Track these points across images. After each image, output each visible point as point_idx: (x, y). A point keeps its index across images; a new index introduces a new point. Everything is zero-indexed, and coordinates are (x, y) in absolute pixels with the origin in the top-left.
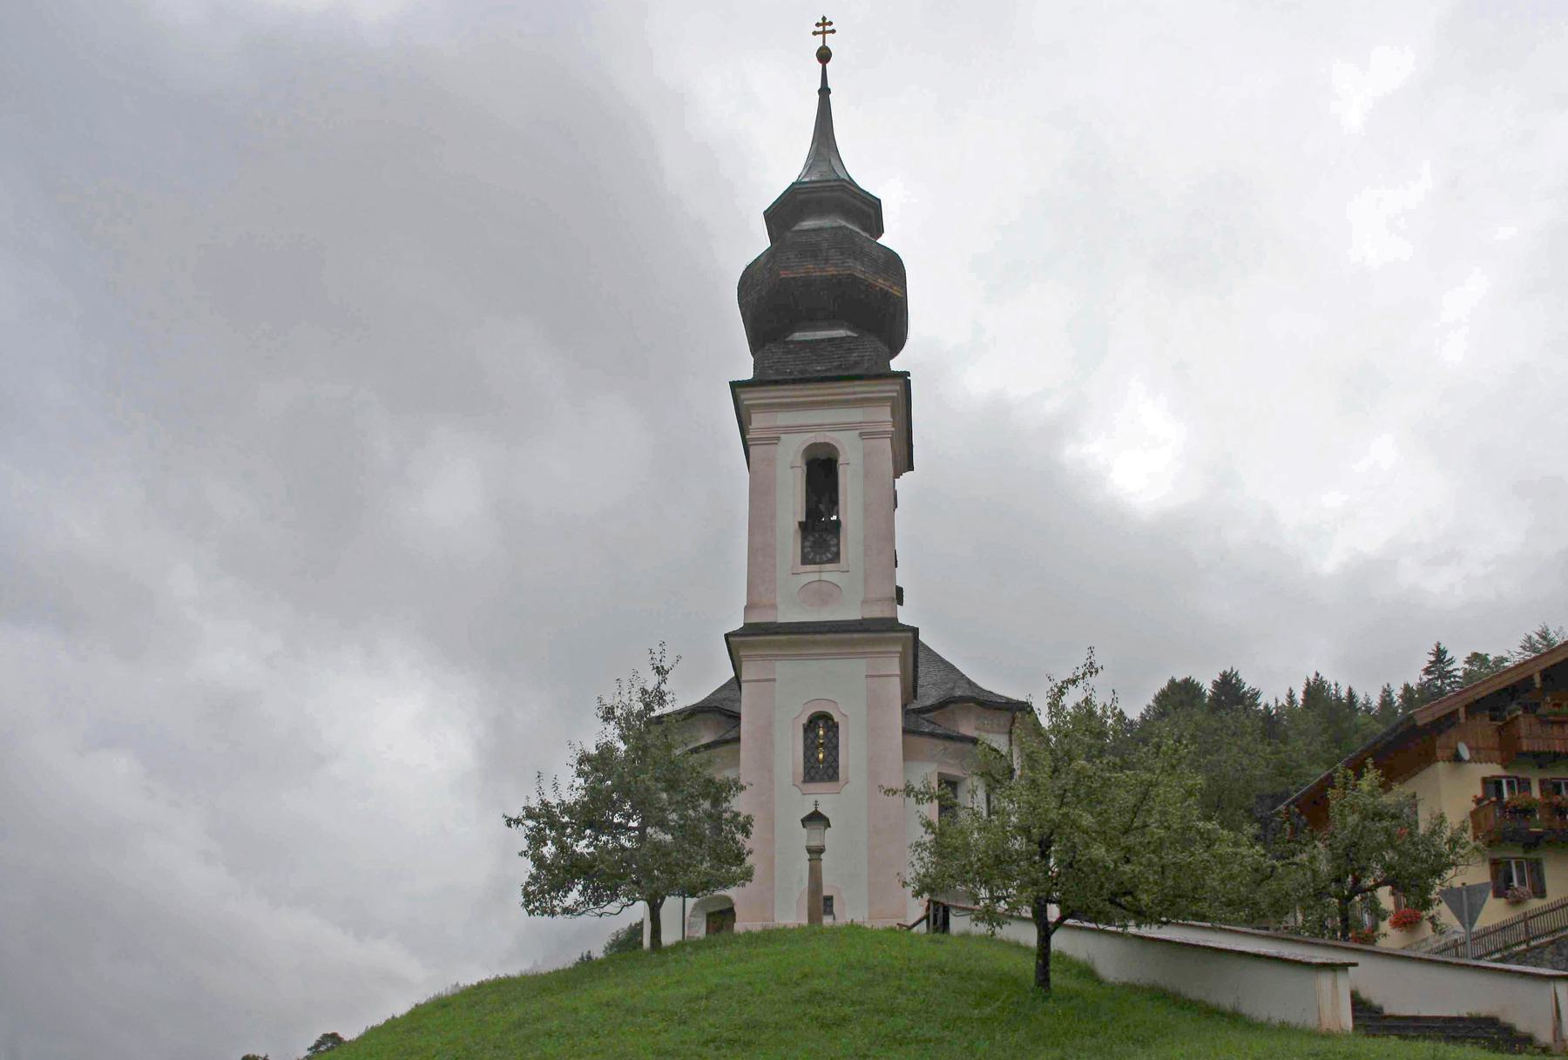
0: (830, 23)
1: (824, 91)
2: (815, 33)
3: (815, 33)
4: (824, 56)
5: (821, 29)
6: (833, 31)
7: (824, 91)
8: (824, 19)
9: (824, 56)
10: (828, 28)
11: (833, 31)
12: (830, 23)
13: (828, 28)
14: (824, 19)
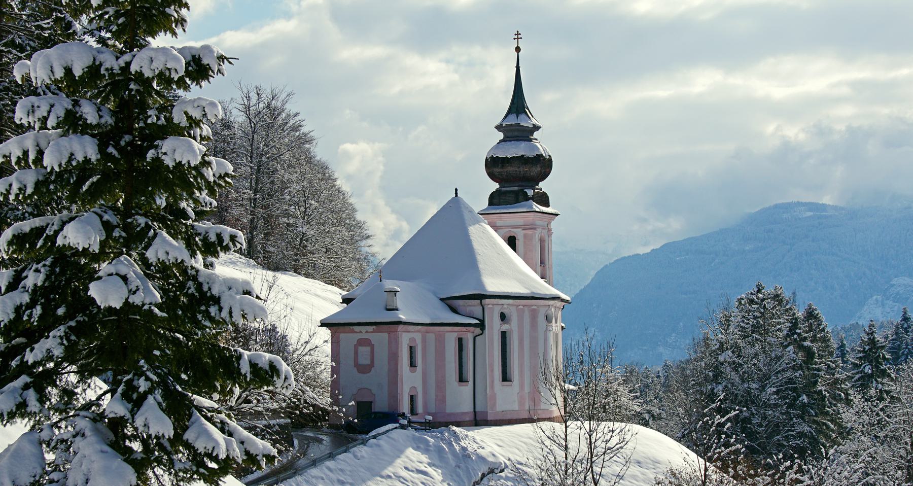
0: (520, 34)
1: (518, 67)
2: (514, 39)
3: (514, 39)
4: (518, 49)
5: (516, 37)
6: (521, 38)
7: (518, 67)
8: (518, 32)
9: (518, 49)
10: (519, 36)
11: (521, 38)
12: (520, 34)
13: (519, 36)
14: (518, 32)
